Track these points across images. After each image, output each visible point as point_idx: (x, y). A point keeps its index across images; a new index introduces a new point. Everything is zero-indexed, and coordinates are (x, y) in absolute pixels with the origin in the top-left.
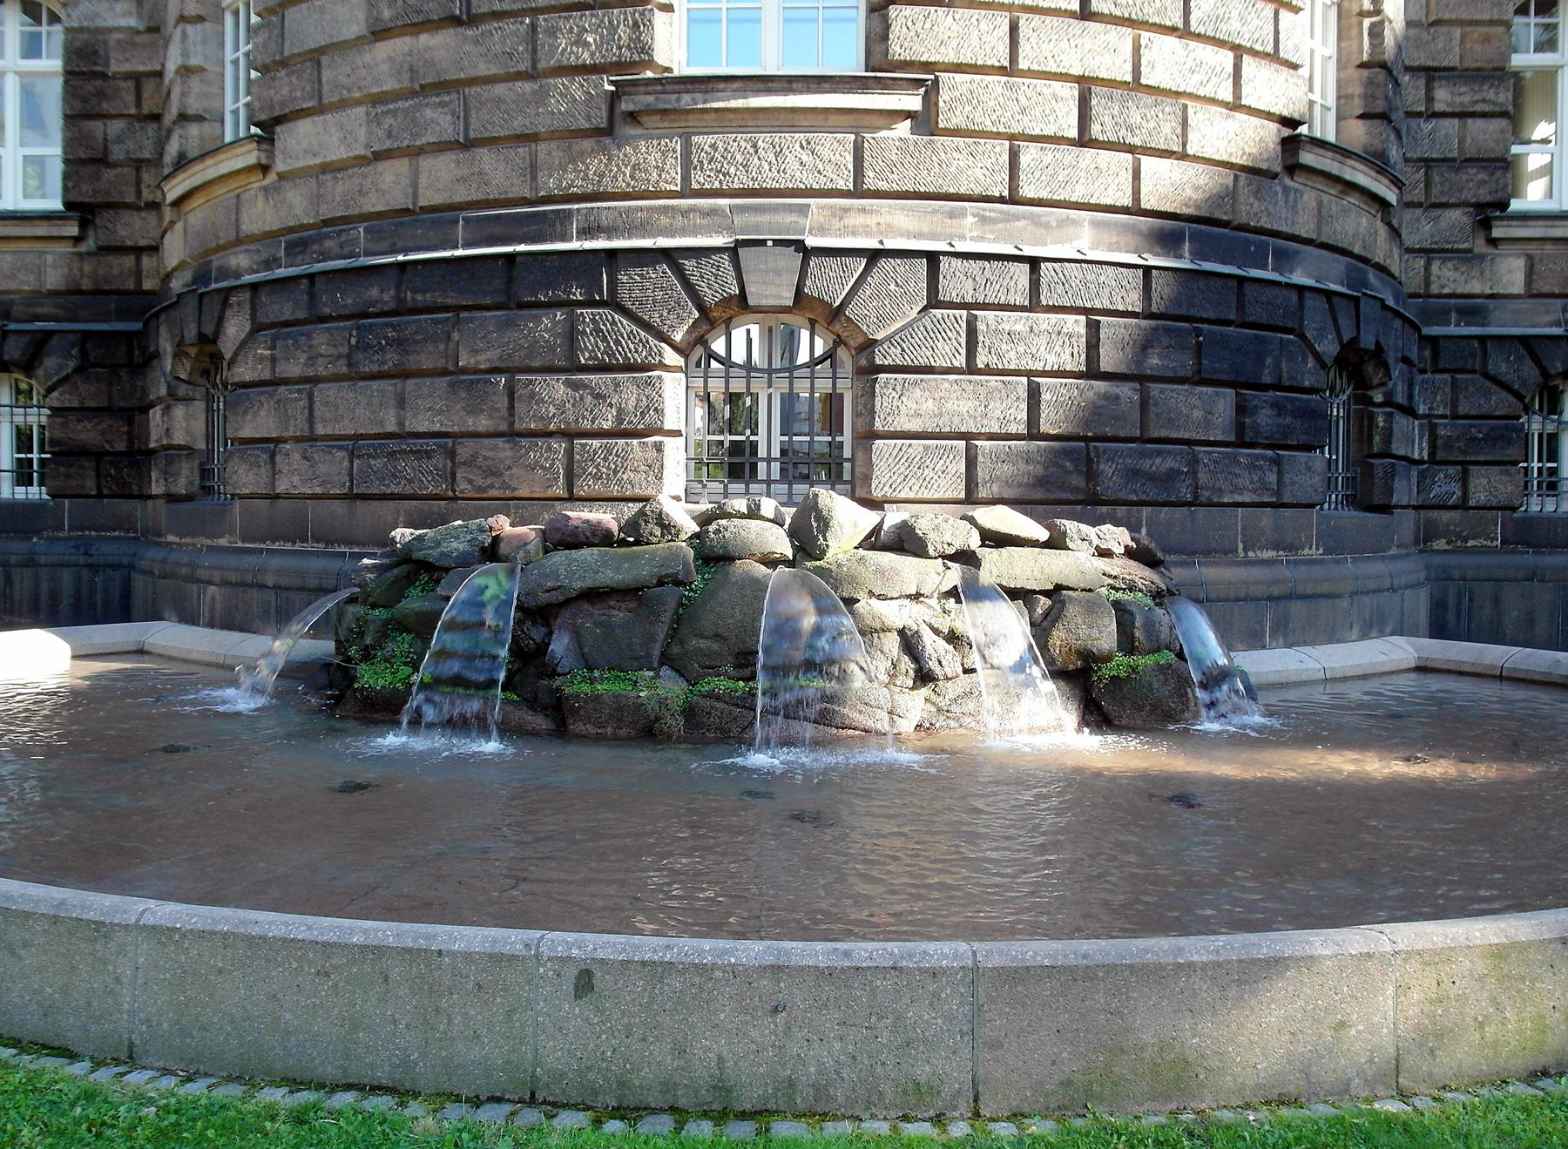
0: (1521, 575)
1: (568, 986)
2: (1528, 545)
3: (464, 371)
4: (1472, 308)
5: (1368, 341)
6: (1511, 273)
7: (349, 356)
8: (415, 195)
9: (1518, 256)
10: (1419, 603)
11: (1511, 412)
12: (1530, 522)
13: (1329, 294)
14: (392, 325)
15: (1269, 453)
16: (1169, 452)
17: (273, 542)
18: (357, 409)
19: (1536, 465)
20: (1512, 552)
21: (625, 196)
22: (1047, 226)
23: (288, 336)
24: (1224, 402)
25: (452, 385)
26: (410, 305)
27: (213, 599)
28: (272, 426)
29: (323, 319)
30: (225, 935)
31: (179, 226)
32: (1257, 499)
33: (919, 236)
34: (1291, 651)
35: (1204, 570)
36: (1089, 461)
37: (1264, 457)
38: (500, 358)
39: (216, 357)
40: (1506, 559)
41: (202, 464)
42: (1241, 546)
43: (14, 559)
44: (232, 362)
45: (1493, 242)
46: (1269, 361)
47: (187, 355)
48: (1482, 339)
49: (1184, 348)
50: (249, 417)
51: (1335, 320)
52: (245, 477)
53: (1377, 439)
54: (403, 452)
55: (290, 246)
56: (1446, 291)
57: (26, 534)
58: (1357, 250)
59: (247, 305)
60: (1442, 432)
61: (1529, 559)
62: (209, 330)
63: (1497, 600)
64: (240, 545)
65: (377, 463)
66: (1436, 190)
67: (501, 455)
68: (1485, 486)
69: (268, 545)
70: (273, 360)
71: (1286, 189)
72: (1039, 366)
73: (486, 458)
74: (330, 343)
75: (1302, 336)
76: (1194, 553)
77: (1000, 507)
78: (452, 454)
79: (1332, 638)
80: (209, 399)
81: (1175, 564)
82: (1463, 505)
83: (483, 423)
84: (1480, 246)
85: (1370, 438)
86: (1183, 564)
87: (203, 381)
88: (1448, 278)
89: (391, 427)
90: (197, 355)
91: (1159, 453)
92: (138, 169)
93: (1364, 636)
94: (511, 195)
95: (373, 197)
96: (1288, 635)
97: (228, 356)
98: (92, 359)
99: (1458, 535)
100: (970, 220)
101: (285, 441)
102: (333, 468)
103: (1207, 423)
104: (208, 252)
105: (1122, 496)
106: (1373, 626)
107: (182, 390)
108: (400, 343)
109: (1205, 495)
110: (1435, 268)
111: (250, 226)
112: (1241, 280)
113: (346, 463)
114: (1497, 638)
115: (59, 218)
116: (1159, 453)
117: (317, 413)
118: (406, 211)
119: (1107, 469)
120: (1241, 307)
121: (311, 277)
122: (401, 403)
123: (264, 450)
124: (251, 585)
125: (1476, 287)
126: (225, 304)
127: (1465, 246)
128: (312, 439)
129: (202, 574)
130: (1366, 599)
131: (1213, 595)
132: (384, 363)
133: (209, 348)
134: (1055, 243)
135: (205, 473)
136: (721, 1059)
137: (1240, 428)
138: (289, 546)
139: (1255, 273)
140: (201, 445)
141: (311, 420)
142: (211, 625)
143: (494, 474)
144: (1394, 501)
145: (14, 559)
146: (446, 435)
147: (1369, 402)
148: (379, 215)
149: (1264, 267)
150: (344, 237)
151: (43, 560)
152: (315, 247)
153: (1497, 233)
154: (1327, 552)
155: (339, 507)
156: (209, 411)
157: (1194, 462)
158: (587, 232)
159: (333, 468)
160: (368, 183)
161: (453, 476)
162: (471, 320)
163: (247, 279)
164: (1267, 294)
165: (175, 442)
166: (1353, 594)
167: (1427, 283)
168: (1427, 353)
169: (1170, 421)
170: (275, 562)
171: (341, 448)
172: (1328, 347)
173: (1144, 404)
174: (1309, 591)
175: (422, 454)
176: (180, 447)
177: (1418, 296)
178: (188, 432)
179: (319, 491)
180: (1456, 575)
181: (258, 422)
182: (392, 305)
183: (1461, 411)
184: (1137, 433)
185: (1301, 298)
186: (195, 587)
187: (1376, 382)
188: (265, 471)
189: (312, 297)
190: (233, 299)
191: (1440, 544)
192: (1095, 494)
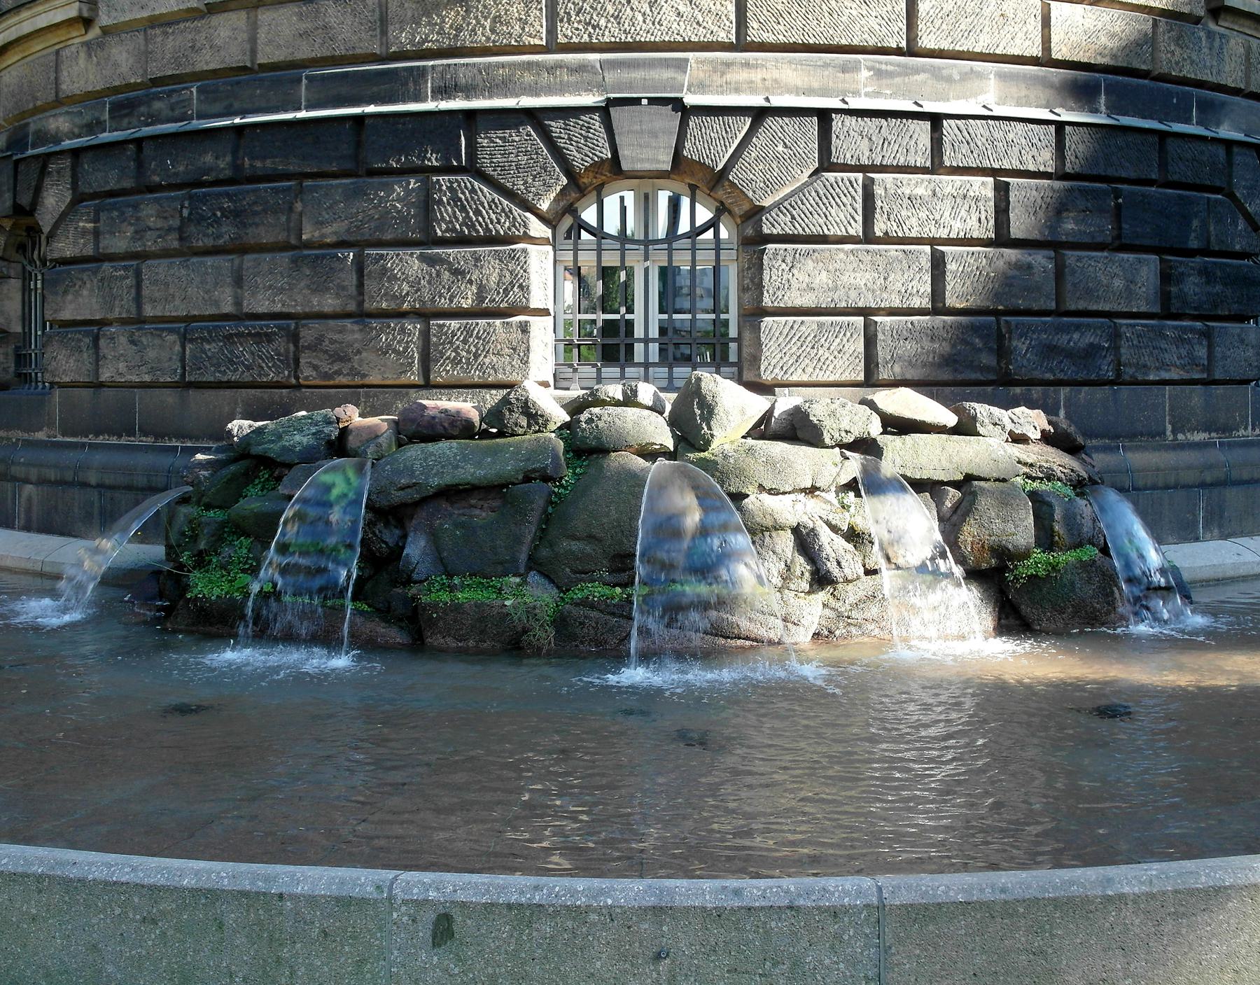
1: (425, 933)
3: (308, 245)
8: (254, 52)
16: (1089, 326)
17: (97, 435)
18: (190, 288)
22: (949, 79)
24: (1148, 269)
25: (294, 261)
26: (248, 172)
27: (29, 499)
28: (96, 307)
29: (152, 189)
32: (1186, 376)
34: (1227, 544)
35: (1129, 455)
36: (1000, 337)
37: (1192, 330)
38: (348, 230)
39: (34, 230)
41: (17, 348)
42: (1169, 427)
44: (51, 236)
46: (1195, 223)
50: (70, 297)
52: (65, 363)
62: (25, 200)
64: (60, 438)
69: (91, 439)
70: (96, 233)
71: (1210, 35)
72: (943, 234)
73: (332, 342)
75: (1231, 196)
76: (1117, 437)
78: (294, 337)
80: (26, 277)
83: (330, 303)
87: (20, 257)
89: (227, 308)
90: (14, 226)
91: (1078, 327)
94: (359, 51)
97: (46, 230)
102: (163, 353)
104: (24, 114)
105: (1037, 374)
108: (237, 215)
109: (1128, 372)
112: (1163, 135)
113: (177, 348)
117: (145, 292)
118: (244, 69)
119: (1020, 345)
120: (1163, 165)
121: (139, 142)
122: (238, 281)
123: (87, 334)
126: (43, 172)
128: (140, 321)
129: (16, 471)
131: (1141, 483)
132: (219, 236)
133: (26, 221)
137: (1165, 298)
138: (114, 440)
140: (17, 328)
141: (138, 300)
142: (27, 528)
149: (1187, 121)
150: (174, 98)
152: (143, 109)
156: (26, 290)
157: (1116, 336)
158: (443, 92)
163: (67, 144)
170: (99, 458)
171: (171, 331)
174: (1246, 476)
179: (147, 378)
181: (81, 302)
182: (228, 173)
184: (1053, 305)
190: (52, 167)
192: (1008, 373)
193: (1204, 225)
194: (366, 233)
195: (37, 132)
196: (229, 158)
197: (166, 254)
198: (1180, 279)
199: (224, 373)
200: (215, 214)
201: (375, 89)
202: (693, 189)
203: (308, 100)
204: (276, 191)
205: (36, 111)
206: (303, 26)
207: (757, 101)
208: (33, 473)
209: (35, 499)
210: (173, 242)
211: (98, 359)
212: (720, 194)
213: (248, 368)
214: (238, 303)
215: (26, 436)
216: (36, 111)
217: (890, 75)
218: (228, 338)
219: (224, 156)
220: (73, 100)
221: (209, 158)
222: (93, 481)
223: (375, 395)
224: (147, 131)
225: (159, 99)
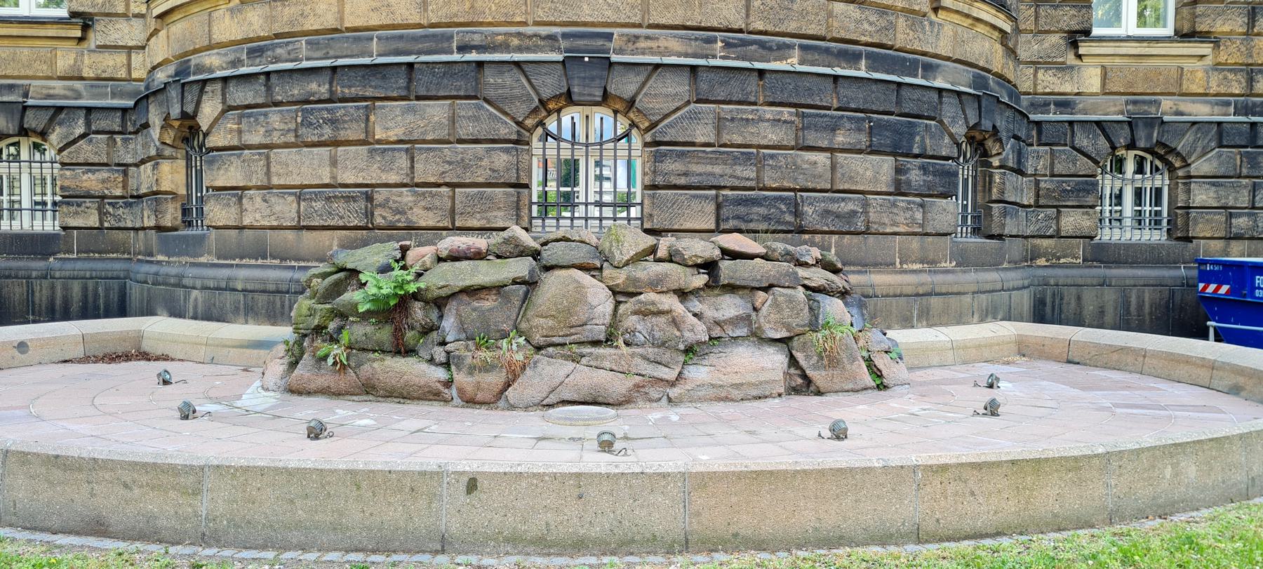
0: (1095, 282)
1: (462, 487)
2: (1101, 262)
3: (379, 142)
4: (1064, 104)
5: (987, 124)
6: (1091, 79)
7: (296, 130)
8: (342, 19)
9: (1096, 66)
10: (1024, 300)
11: (1090, 172)
12: (1103, 247)
13: (959, 94)
14: (327, 109)
15: (918, 200)
17: (242, 258)
18: (308, 166)
19: (1148, 208)
20: (1090, 267)
21: (490, 24)
22: (770, 49)
23: (250, 116)
24: (886, 164)
25: (370, 151)
26: (340, 96)
27: (196, 299)
28: (240, 178)
29: (276, 104)
30: (262, 469)
31: (163, 33)
32: (910, 230)
33: (686, 55)
34: (930, 330)
35: (873, 276)
36: (797, 205)
37: (914, 203)
39: (194, 130)
40: (1087, 271)
41: (183, 205)
43: (34, 274)
44: (206, 135)
45: (1079, 57)
46: (918, 138)
47: (171, 126)
48: (1071, 123)
49: (859, 130)
50: (222, 172)
51: (964, 111)
52: (218, 213)
53: (995, 190)
54: (335, 197)
55: (251, 52)
56: (1048, 90)
57: (45, 255)
58: (981, 64)
59: (219, 93)
60: (1042, 185)
61: (1102, 271)
62: (189, 109)
63: (1079, 298)
64: (216, 261)
65: (318, 205)
66: (1042, 21)
67: (406, 199)
68: (1072, 221)
69: (237, 261)
70: (240, 132)
71: (932, 23)
72: (764, 142)
73: (395, 202)
74: (283, 121)
75: (941, 122)
77: (736, 235)
78: (369, 198)
79: (960, 320)
80: (188, 158)
81: (853, 272)
82: (1057, 235)
83: (393, 178)
84: (1070, 59)
85: (990, 190)
86: (859, 272)
87: (183, 146)
88: (1049, 82)
90: (180, 126)
91: (843, 199)
93: (982, 320)
95: (311, 20)
96: (928, 318)
97: (204, 128)
98: (93, 128)
99: (1054, 255)
100: (720, 44)
101: (249, 188)
102: (286, 209)
103: (876, 180)
104: (186, 54)
105: (818, 227)
106: (988, 314)
107: (168, 151)
108: (333, 122)
109: (874, 227)
110: (1040, 74)
111: (218, 36)
112: (899, 84)
113: (295, 205)
114: (1079, 322)
115: (66, 24)
116: (843, 199)
117: (273, 169)
118: (336, 30)
119: (808, 210)
120: (898, 103)
121: (268, 74)
122: (334, 163)
123: (234, 195)
124: (225, 289)
125: (1068, 88)
126: (202, 91)
127: (1061, 60)
128: (269, 187)
129: (186, 281)
130: (983, 296)
132: (322, 135)
133: (188, 123)
134: (775, 60)
135: (185, 211)
136: (547, 524)
137: (898, 183)
138: (253, 262)
139: (908, 80)
140: (183, 191)
141: (268, 173)
142: (195, 318)
143: (400, 213)
144: (1006, 232)
145: (34, 274)
146: (367, 186)
147: (990, 165)
148: (317, 32)
149: (915, 76)
151: (57, 274)
152: (269, 53)
153: (1081, 51)
154: (958, 265)
155: (290, 235)
156: (189, 167)
157: (866, 205)
158: (463, 49)
159: (286, 209)
160: (307, 9)
161: (372, 214)
162: (383, 107)
163: (219, 74)
164: (917, 94)
165: (163, 189)
166: (974, 293)
167: (1035, 85)
168: (1034, 133)
169: (851, 178)
170: (243, 273)
171: (290, 194)
172: (959, 130)
173: (833, 167)
174: (944, 291)
175: (348, 199)
176: (166, 193)
177: (1029, 94)
178: (172, 182)
179: (275, 223)
180: (1052, 282)
181: (229, 174)
182: (327, 96)
183: (1056, 171)
184: (829, 187)
185: (940, 97)
186: (181, 291)
187: (994, 152)
188: (234, 210)
189: (269, 88)
190: (208, 88)
191: (1042, 262)
192: (801, 226)
193: (923, 139)
194: (415, 136)
195: (197, 65)
196: (327, 86)
197: (286, 145)
198: (906, 172)
202: (616, 112)
204: (358, 108)
205: (195, 51)
207: (656, 59)
208: (198, 283)
209: (200, 300)
210: (291, 138)
211: (242, 211)
212: (631, 115)
214: (334, 177)
215: (192, 260)
216: (195, 51)
217: (735, 46)
218: (328, 199)
220: (221, 45)
222: (239, 288)
224: (272, 67)
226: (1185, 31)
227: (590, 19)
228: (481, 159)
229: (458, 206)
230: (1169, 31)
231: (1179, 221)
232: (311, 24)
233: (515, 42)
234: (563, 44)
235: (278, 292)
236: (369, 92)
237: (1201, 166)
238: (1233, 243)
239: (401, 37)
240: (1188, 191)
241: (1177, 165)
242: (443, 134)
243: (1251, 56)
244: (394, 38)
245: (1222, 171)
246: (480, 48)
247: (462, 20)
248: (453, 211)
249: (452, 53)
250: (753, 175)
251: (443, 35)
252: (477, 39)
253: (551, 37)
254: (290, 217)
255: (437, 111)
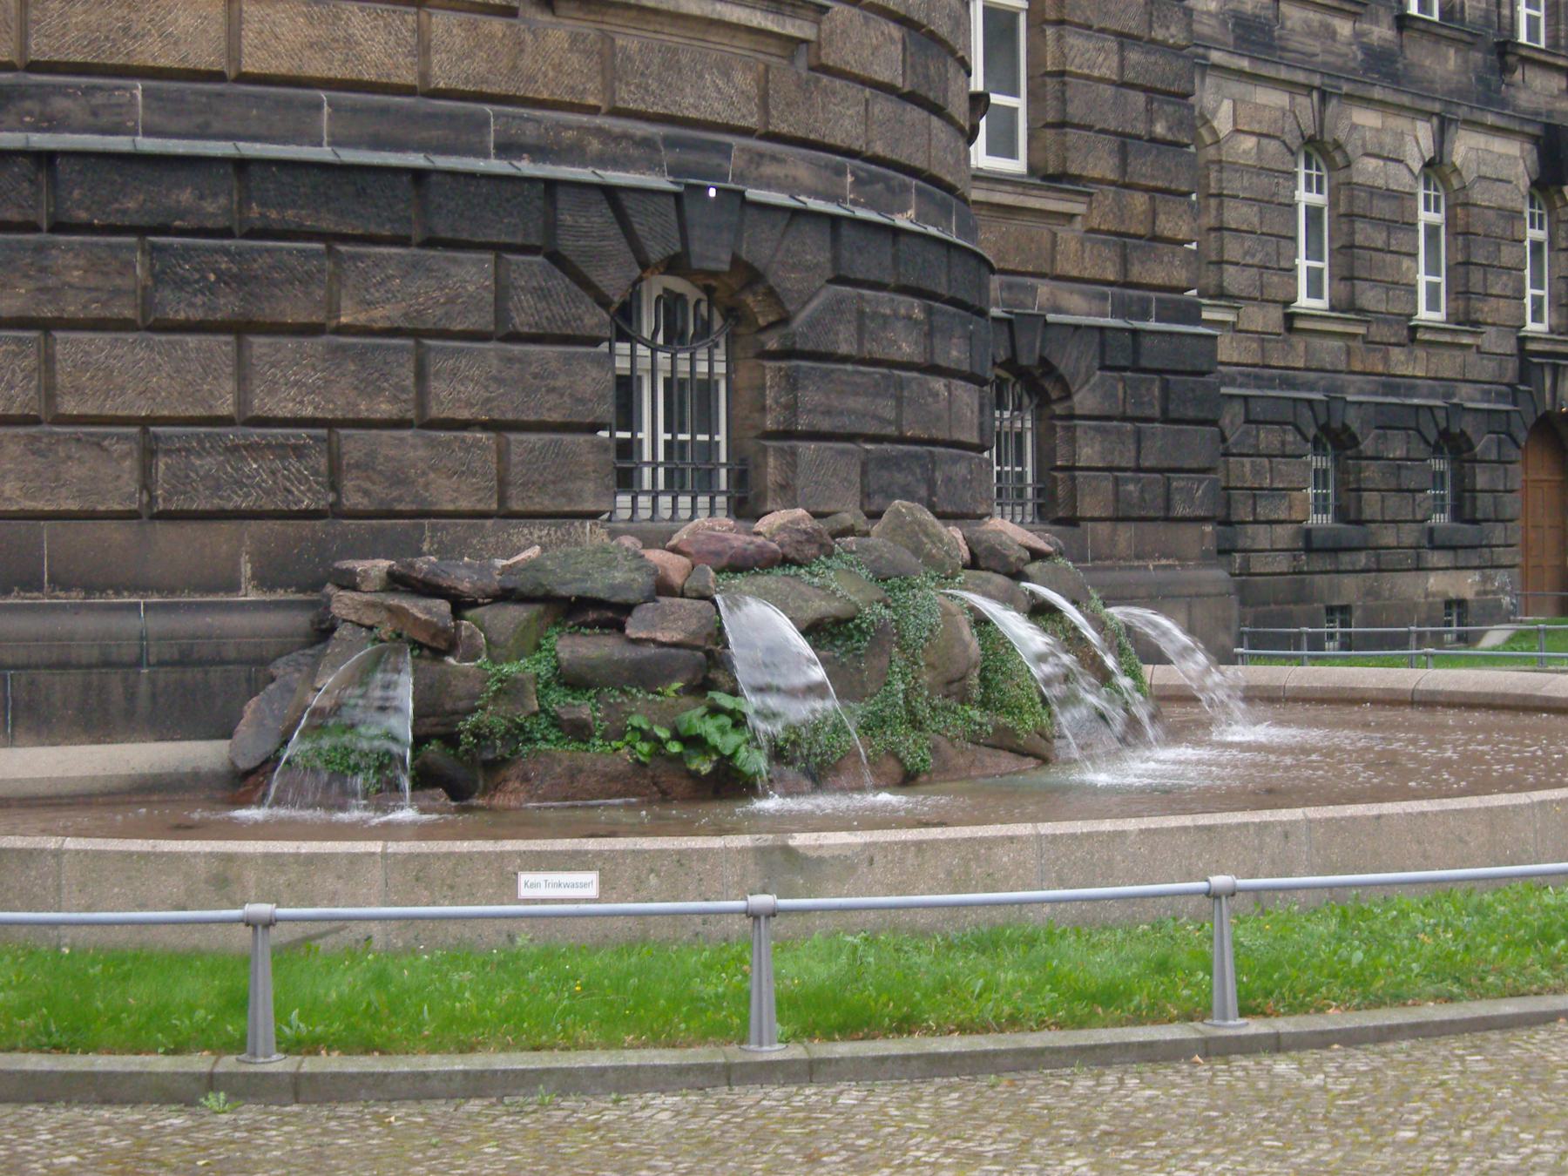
14: (226, 251)
26: (258, 225)
38: (406, 315)
54: (251, 447)
73: (388, 459)
83: (384, 409)
89: (226, 408)
92: (1352, 222)
94: (395, 80)
118: (218, 77)
150: (99, 99)
155: (115, 533)
158: (507, 149)
199: (229, 499)
200: (205, 278)
201: (425, 134)
203: (331, 135)
206: (314, 33)
213: (267, 492)
219: (215, 195)
221: (186, 197)
223: (444, 528)
225: (66, 95)
226: (1051, 171)
227: (693, 114)
228: (554, 375)
229: (516, 474)
230: (1017, 166)
231: (1061, 491)
232: (152, 53)
233: (595, 145)
234: (668, 157)
235: (107, 664)
236: (328, 223)
237: (1085, 400)
238: (1121, 526)
239: (384, 111)
240: (1072, 441)
241: (1054, 396)
242: (481, 320)
243: (1123, 222)
244: (369, 110)
245: (1107, 409)
246: (540, 153)
247: (495, 90)
248: (503, 483)
249: (486, 156)
250: (890, 414)
251: (470, 116)
252: (530, 133)
253: (646, 142)
254: (121, 489)
255: (471, 275)
